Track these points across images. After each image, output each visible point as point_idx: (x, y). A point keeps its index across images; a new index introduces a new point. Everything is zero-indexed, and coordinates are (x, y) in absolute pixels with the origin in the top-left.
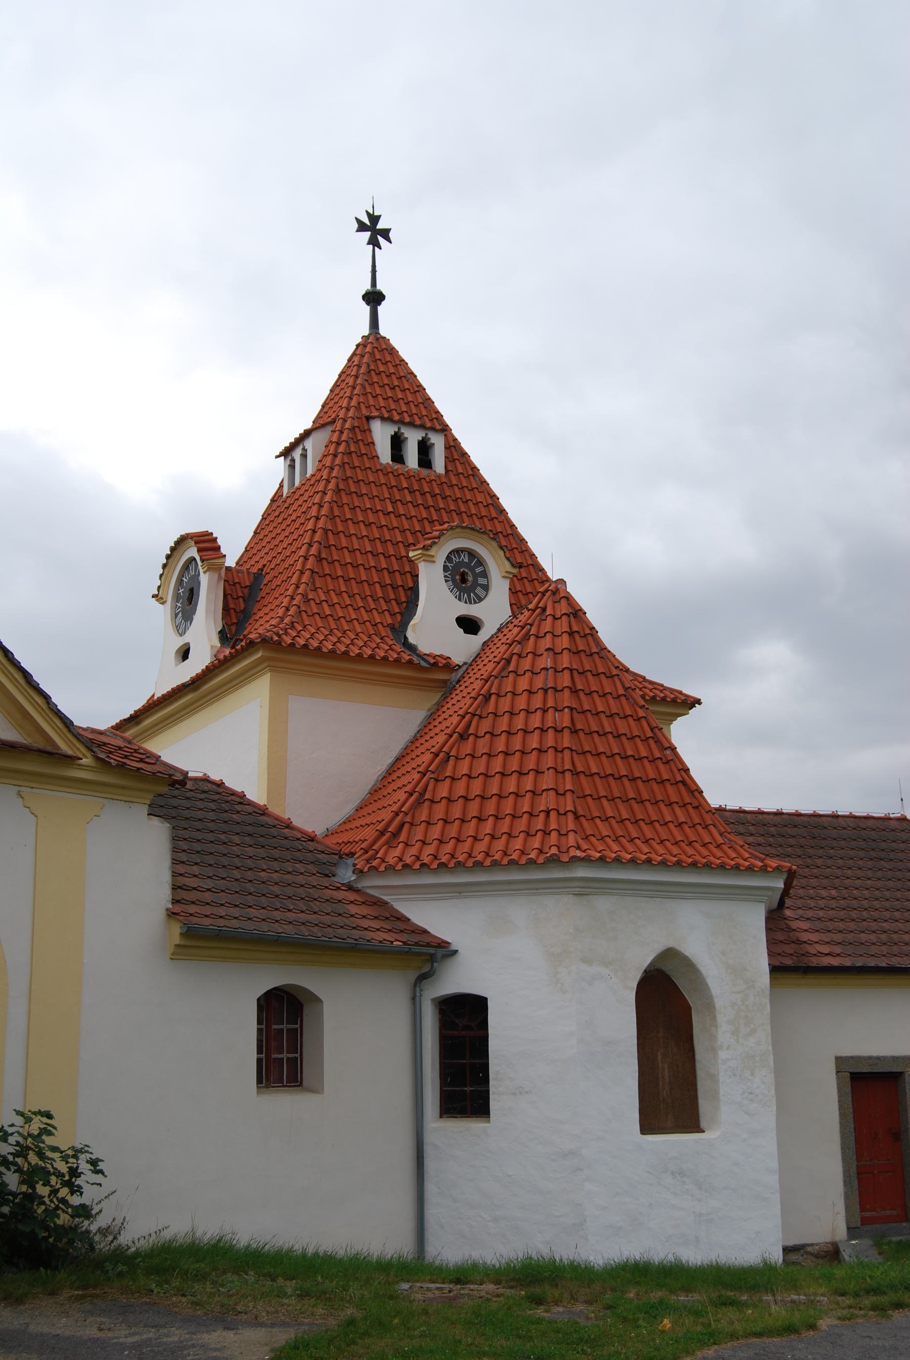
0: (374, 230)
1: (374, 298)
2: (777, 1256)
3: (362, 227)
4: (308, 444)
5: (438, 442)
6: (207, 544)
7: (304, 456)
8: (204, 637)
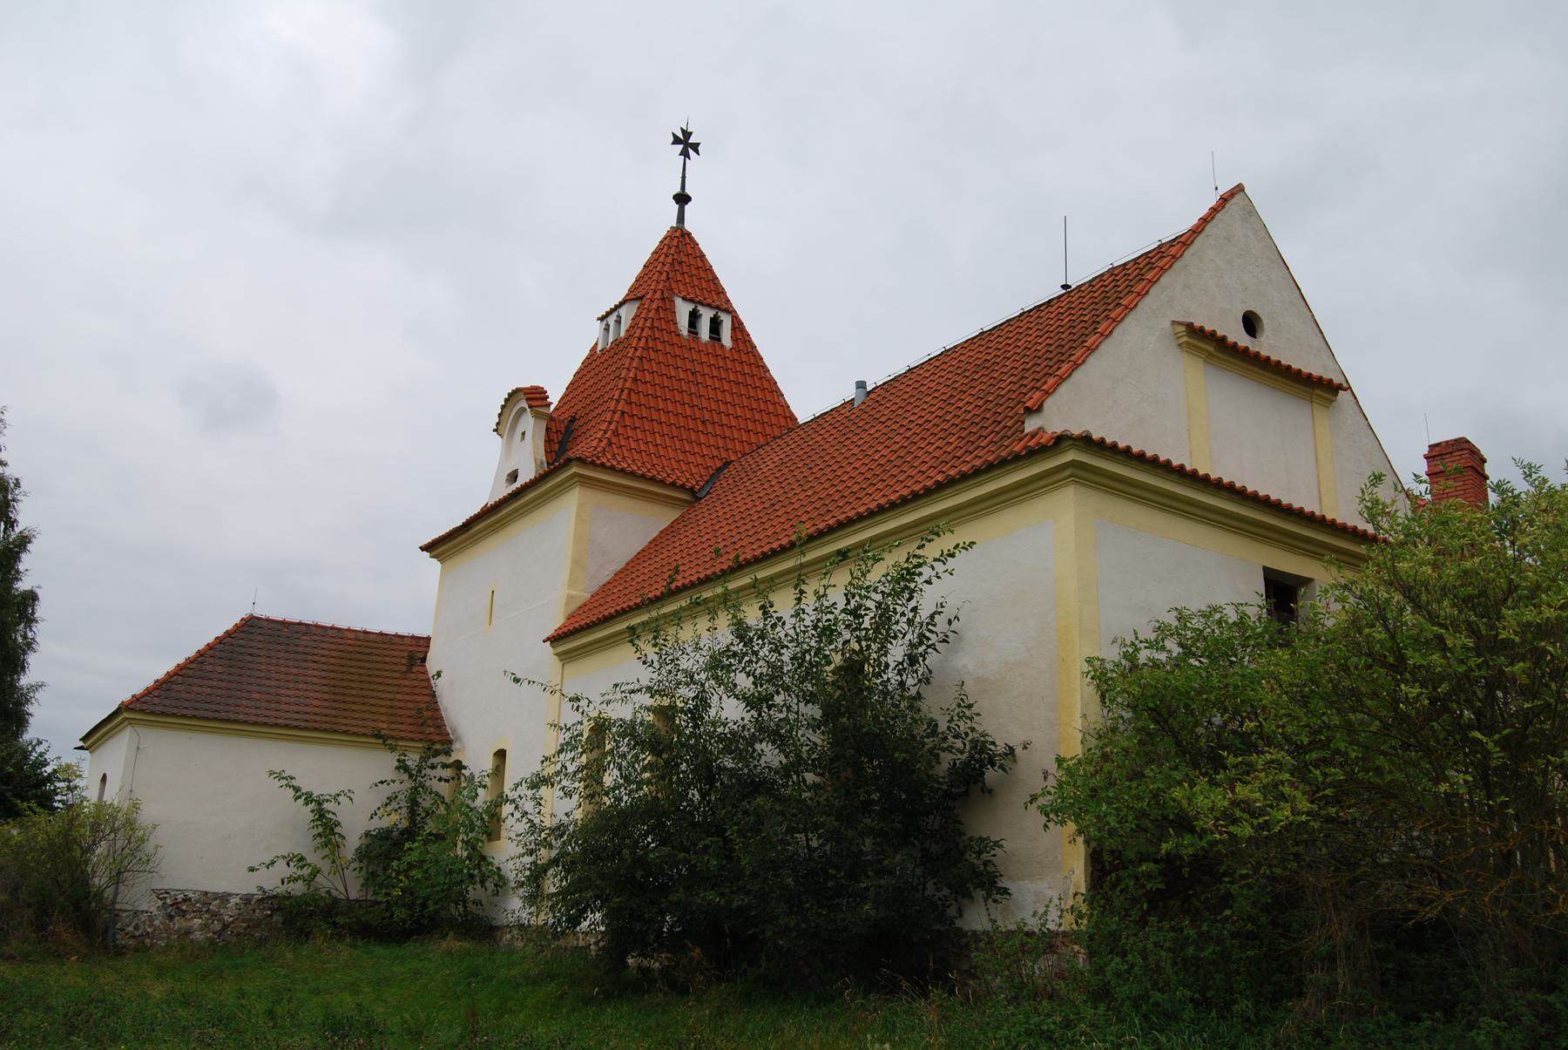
0: (686, 143)
1: (682, 199)
2: (23, 586)
3: (676, 141)
4: (623, 311)
5: (726, 322)
6: (536, 396)
7: (618, 322)
8: (528, 459)
